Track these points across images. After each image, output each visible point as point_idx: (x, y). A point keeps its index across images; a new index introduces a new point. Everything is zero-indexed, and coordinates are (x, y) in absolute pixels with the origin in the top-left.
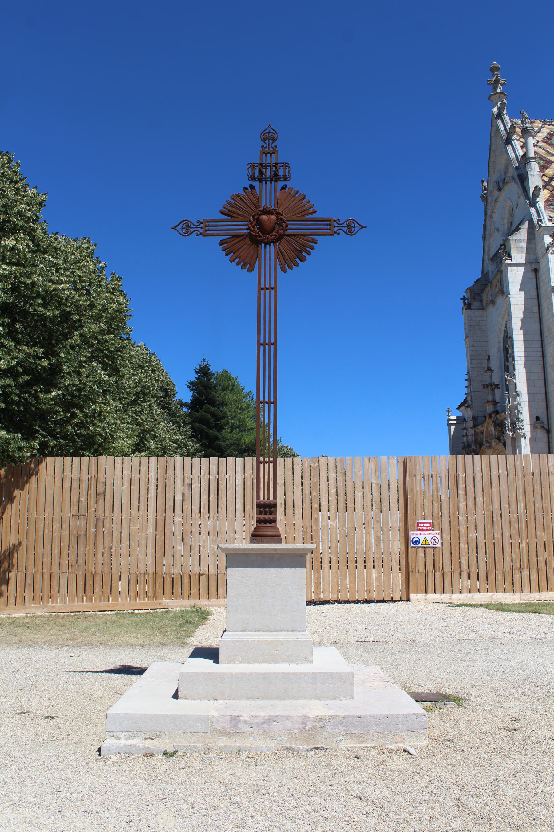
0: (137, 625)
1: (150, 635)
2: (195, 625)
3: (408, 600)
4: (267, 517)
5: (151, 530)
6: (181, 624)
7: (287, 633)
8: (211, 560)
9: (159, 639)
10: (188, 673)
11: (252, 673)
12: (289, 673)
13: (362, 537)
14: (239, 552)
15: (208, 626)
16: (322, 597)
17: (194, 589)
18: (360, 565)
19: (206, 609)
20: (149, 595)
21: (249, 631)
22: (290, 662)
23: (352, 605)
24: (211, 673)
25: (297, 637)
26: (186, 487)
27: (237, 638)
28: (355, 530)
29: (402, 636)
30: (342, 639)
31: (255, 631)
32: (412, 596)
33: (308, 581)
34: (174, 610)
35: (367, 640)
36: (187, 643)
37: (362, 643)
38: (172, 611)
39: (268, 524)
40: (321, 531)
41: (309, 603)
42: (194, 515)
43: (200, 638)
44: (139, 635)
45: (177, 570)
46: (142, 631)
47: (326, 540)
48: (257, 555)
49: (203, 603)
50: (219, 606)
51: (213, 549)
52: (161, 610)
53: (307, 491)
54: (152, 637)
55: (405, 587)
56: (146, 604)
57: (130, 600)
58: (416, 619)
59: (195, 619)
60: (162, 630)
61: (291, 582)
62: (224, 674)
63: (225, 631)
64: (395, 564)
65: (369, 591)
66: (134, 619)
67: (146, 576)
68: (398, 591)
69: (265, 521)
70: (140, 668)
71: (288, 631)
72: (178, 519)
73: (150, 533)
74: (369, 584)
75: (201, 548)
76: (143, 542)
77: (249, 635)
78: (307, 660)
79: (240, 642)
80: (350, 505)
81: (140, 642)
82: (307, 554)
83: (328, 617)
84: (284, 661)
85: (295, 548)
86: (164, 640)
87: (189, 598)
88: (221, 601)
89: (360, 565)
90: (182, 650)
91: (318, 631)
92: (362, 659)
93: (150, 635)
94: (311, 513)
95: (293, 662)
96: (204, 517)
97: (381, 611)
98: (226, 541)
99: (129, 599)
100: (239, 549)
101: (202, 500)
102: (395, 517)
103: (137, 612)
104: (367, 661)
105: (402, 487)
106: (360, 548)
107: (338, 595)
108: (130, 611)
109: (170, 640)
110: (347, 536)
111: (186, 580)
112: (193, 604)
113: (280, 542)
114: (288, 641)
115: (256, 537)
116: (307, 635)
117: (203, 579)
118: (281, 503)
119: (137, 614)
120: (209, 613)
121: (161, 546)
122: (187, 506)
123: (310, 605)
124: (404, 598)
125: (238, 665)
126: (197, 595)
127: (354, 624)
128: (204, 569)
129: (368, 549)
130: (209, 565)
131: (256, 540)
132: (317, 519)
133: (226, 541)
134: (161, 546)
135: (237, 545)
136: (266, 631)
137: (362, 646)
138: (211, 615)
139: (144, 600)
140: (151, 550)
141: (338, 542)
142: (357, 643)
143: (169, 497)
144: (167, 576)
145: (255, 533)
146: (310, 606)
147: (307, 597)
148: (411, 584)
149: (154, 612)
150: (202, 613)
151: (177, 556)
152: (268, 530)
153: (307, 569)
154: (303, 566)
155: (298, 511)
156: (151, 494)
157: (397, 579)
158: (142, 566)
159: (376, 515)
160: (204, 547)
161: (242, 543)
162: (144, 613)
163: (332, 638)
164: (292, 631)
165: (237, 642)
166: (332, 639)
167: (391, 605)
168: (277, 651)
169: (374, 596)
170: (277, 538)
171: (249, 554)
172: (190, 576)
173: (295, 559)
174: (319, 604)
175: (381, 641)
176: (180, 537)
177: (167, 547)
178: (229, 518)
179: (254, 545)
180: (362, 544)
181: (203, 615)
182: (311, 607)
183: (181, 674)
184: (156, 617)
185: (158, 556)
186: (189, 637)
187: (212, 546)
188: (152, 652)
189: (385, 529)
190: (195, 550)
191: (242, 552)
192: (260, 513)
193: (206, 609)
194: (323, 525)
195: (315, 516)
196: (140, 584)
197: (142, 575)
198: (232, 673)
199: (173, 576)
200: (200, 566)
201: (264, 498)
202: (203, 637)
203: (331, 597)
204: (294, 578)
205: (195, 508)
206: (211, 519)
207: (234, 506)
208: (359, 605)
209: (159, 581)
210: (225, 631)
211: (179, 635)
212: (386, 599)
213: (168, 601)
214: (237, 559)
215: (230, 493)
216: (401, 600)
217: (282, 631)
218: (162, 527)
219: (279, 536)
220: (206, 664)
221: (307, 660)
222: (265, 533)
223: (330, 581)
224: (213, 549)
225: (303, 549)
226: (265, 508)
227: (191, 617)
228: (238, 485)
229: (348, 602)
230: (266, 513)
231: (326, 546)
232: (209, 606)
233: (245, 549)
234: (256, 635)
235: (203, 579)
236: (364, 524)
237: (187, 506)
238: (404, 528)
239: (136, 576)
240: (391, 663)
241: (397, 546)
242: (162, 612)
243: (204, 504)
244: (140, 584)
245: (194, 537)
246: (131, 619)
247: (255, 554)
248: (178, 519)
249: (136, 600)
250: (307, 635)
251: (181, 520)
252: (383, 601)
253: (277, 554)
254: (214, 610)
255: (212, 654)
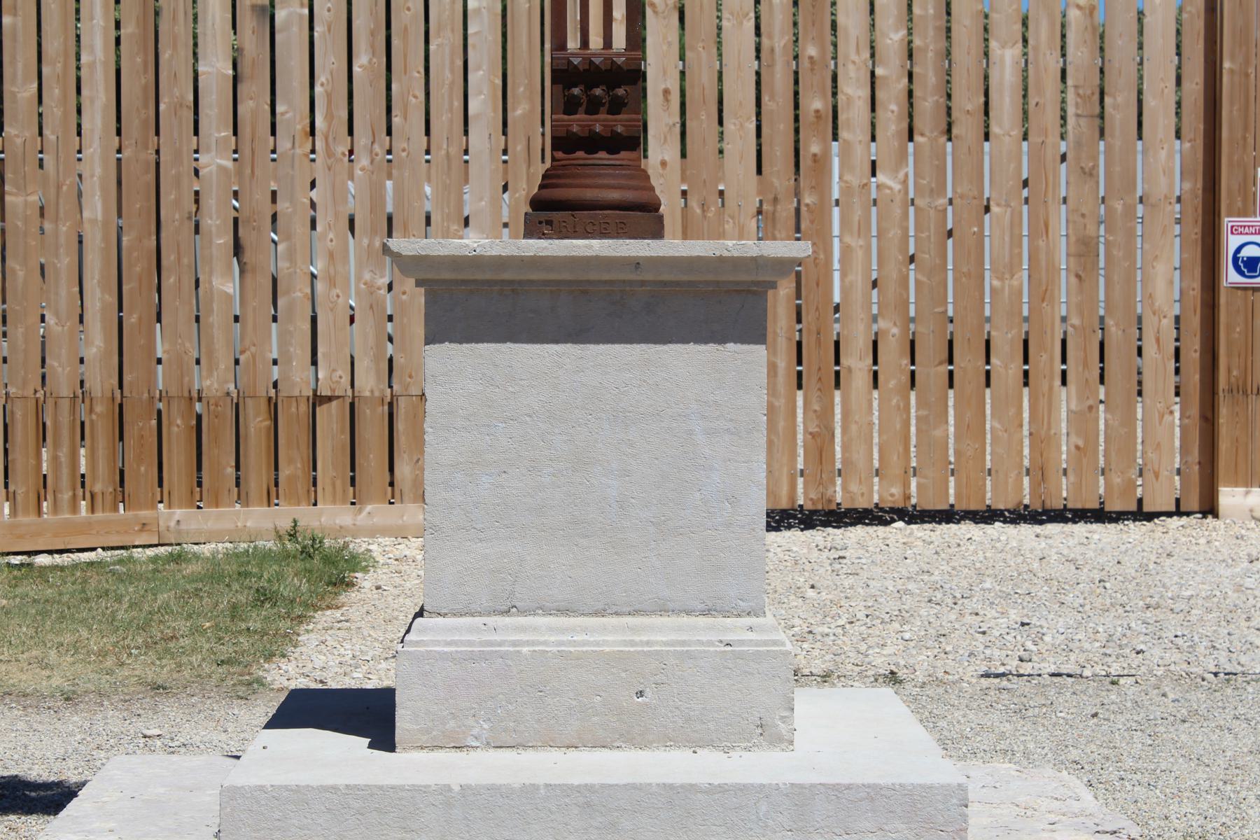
0: (44, 614)
1: (103, 654)
2: (298, 611)
3: (1210, 509)
4: (600, 123)
5: (96, 207)
6: (234, 607)
7: (685, 620)
8: (363, 339)
9: (143, 667)
10: (261, 788)
11: (535, 787)
12: (692, 788)
13: (1016, 241)
14: (479, 276)
15: (354, 613)
16: (839, 495)
17: (290, 461)
18: (1006, 365)
19: (346, 546)
20: (98, 488)
21: (523, 612)
22: (695, 744)
23: (967, 529)
24: (357, 788)
25: (728, 637)
26: (248, 22)
27: (470, 643)
28: (987, 209)
29: (1176, 656)
30: (922, 663)
31: (548, 612)
32: (1228, 497)
33: (781, 424)
34: (206, 550)
35: (1027, 668)
36: (260, 681)
37: (1005, 683)
38: (197, 557)
39: (602, 154)
40: (836, 211)
41: (779, 519)
42: (284, 144)
43: (320, 660)
44: (53, 654)
45: (214, 382)
46: (68, 638)
47: (860, 253)
48: (553, 288)
49: (329, 518)
50: (401, 533)
51: (371, 288)
52: (150, 552)
53: (777, 39)
54: (110, 662)
55: (1195, 455)
56: (86, 527)
57: (14, 512)
58: (1239, 588)
59: (294, 583)
60: (155, 632)
61: (703, 405)
62: (415, 789)
63: (420, 614)
64: (1157, 361)
65: (1039, 472)
66: (30, 589)
67: (83, 409)
68: (1164, 473)
69: (592, 143)
70: (59, 784)
71: (689, 613)
72: (215, 161)
73: (93, 221)
74: (1042, 441)
75: (320, 286)
76: (64, 262)
77: (523, 629)
78: (770, 732)
79: (483, 656)
80: (967, 102)
81: (56, 681)
82: (773, 285)
83: (864, 575)
84: (669, 740)
85: (721, 259)
86: (163, 672)
87: (272, 495)
88: (409, 513)
89: (1006, 365)
90: (239, 709)
91: (819, 630)
92: (1003, 745)
93: (103, 654)
94: (796, 139)
95: (711, 744)
96: (329, 153)
97: (1091, 554)
98: (428, 221)
99: (7, 506)
100: (476, 262)
101: (321, 78)
102: (1163, 154)
103: (43, 560)
104: (1026, 754)
105: (1200, 25)
106: (1004, 292)
107: (906, 485)
108: (16, 560)
109: (186, 673)
110: (950, 234)
111: (256, 423)
112: (285, 525)
113: (656, 231)
114: (690, 655)
115: (549, 210)
116: (766, 631)
117: (331, 420)
118: (666, 92)
119: (43, 569)
120: (357, 563)
121: (145, 278)
122: (254, 103)
123: (789, 527)
124: (1193, 503)
125: (472, 753)
126: (302, 486)
127: (971, 605)
128: (331, 377)
129: (1042, 293)
130: (349, 362)
131: (549, 223)
132: (821, 163)
133: (428, 221)
134: (145, 278)
135: (473, 243)
136: (596, 614)
137: (1008, 693)
138: (365, 570)
139: (74, 508)
140: (98, 298)
141: (912, 259)
142: (985, 682)
143: (174, 59)
144: (174, 405)
145: (548, 193)
146: (786, 534)
147: (771, 493)
148: (1224, 446)
149: (121, 562)
150: (328, 560)
151: (216, 319)
152: (601, 180)
153: (772, 351)
154: (755, 333)
155: (740, 127)
156: (92, 50)
157: (1165, 427)
158: (61, 368)
159: (1078, 144)
160: (332, 283)
161: (490, 234)
162: (75, 566)
163: (878, 661)
164: (706, 613)
165: (472, 658)
166: (881, 661)
167: (1135, 530)
168: (640, 694)
169: (1063, 492)
170: (642, 215)
171: (520, 282)
172: (273, 407)
173: (717, 306)
174: (826, 524)
175: (1087, 673)
176: (224, 240)
177: (169, 281)
178: (438, 155)
179: (543, 243)
180: (1018, 272)
181: (333, 572)
182: (793, 538)
183: (230, 794)
184: (130, 578)
185: (131, 320)
186: (269, 657)
187: (367, 276)
188: (111, 719)
189: (1119, 206)
190: (295, 296)
191: (488, 276)
192: (570, 106)
193: (346, 546)
194: (846, 189)
195: (812, 147)
196: (56, 445)
197: (65, 405)
198: (448, 788)
199: (198, 407)
200: (314, 362)
201: (585, 43)
202: (328, 655)
203: (876, 494)
204: (720, 384)
205: (291, 111)
206: (363, 161)
207: (458, 104)
208: (997, 529)
209: (140, 427)
210: (420, 614)
211: (226, 651)
212: (1114, 506)
213: (179, 513)
214: (472, 305)
215: (444, 45)
216: (1179, 512)
217: (663, 610)
218: (146, 195)
219: (650, 208)
220: (336, 755)
221: (770, 732)
222: (590, 194)
223: (870, 432)
224: (371, 288)
225: (757, 263)
226: (589, 87)
227: (280, 577)
228: (478, 11)
229: (948, 516)
230: (593, 107)
231: (858, 279)
232: (356, 532)
233: (501, 263)
234: (551, 629)
235: (331, 420)
236: (1025, 183)
237: (254, 103)
238: (1199, 201)
239: (39, 409)
240: (1129, 763)
241: (1165, 284)
242: (154, 560)
243: (329, 96)
244: (56, 445)
245: (288, 237)
246: (19, 591)
247: (547, 283)
248: (215, 161)
249: (39, 512)
250: (766, 631)
251: (229, 164)
252: (1100, 515)
253: (643, 283)
254: (377, 547)
255: (367, 715)
